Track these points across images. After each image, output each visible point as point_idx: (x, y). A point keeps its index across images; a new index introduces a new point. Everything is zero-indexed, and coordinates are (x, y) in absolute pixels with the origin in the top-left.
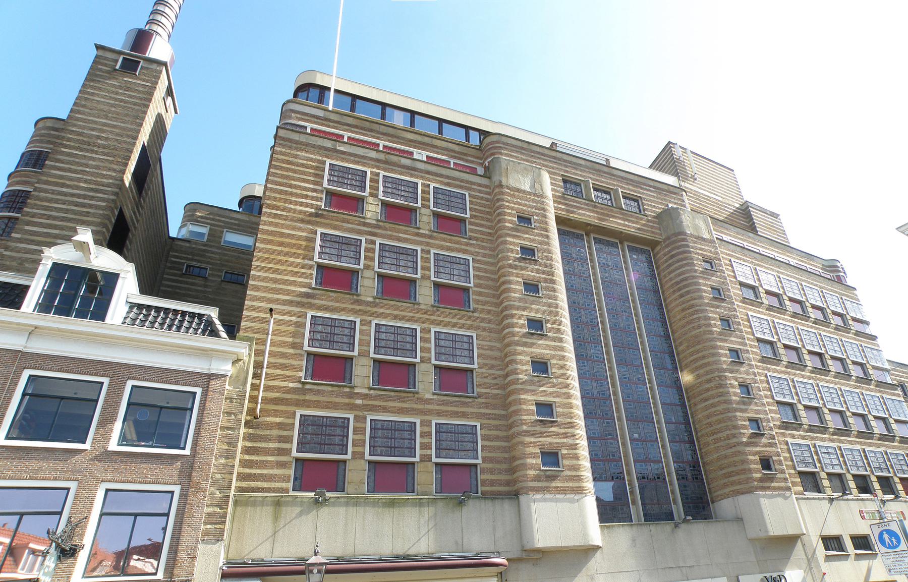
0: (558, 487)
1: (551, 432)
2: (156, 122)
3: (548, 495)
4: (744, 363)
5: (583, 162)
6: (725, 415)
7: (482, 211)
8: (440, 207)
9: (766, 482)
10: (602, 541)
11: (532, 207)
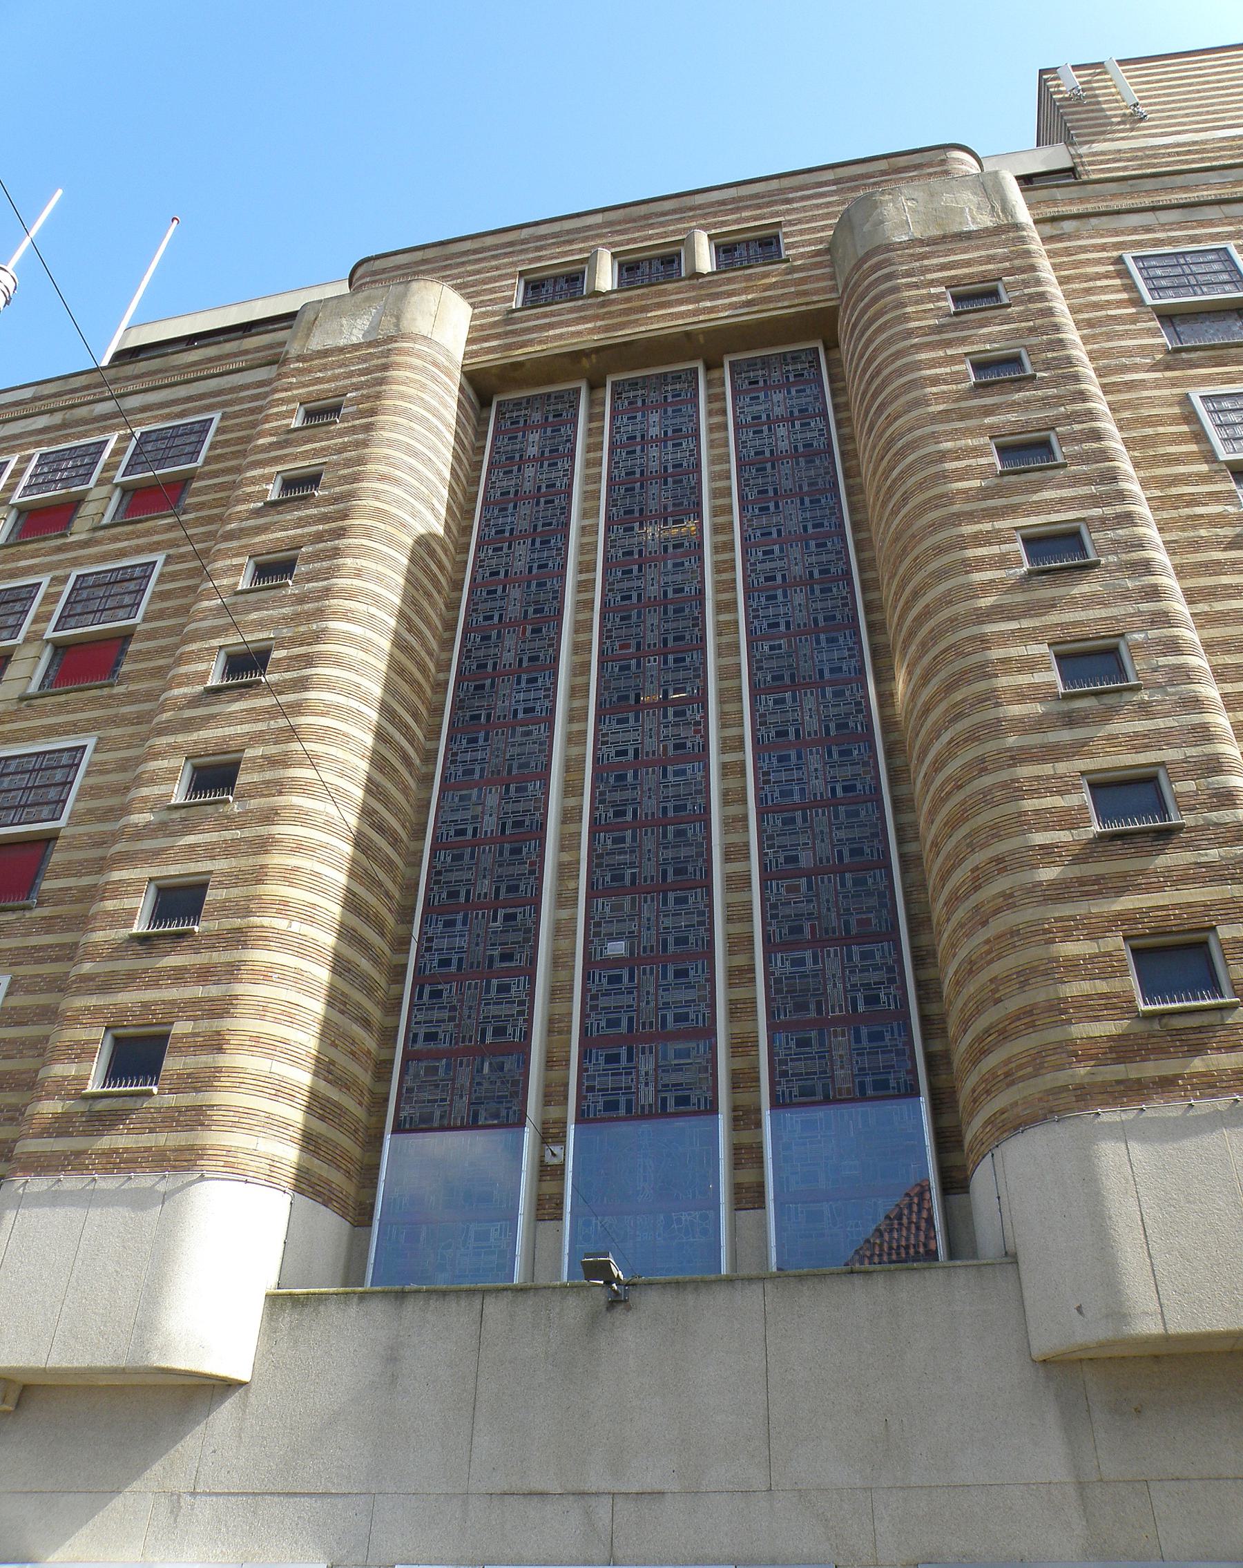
0: (116, 1151)
1: (159, 970)
2: (1231, 549)
3: (71, 1182)
4: (1096, 564)
5: (598, 219)
6: (968, 790)
7: (238, 438)
8: (139, 470)
9: (1160, 1052)
10: (263, 1355)
11: (336, 378)
